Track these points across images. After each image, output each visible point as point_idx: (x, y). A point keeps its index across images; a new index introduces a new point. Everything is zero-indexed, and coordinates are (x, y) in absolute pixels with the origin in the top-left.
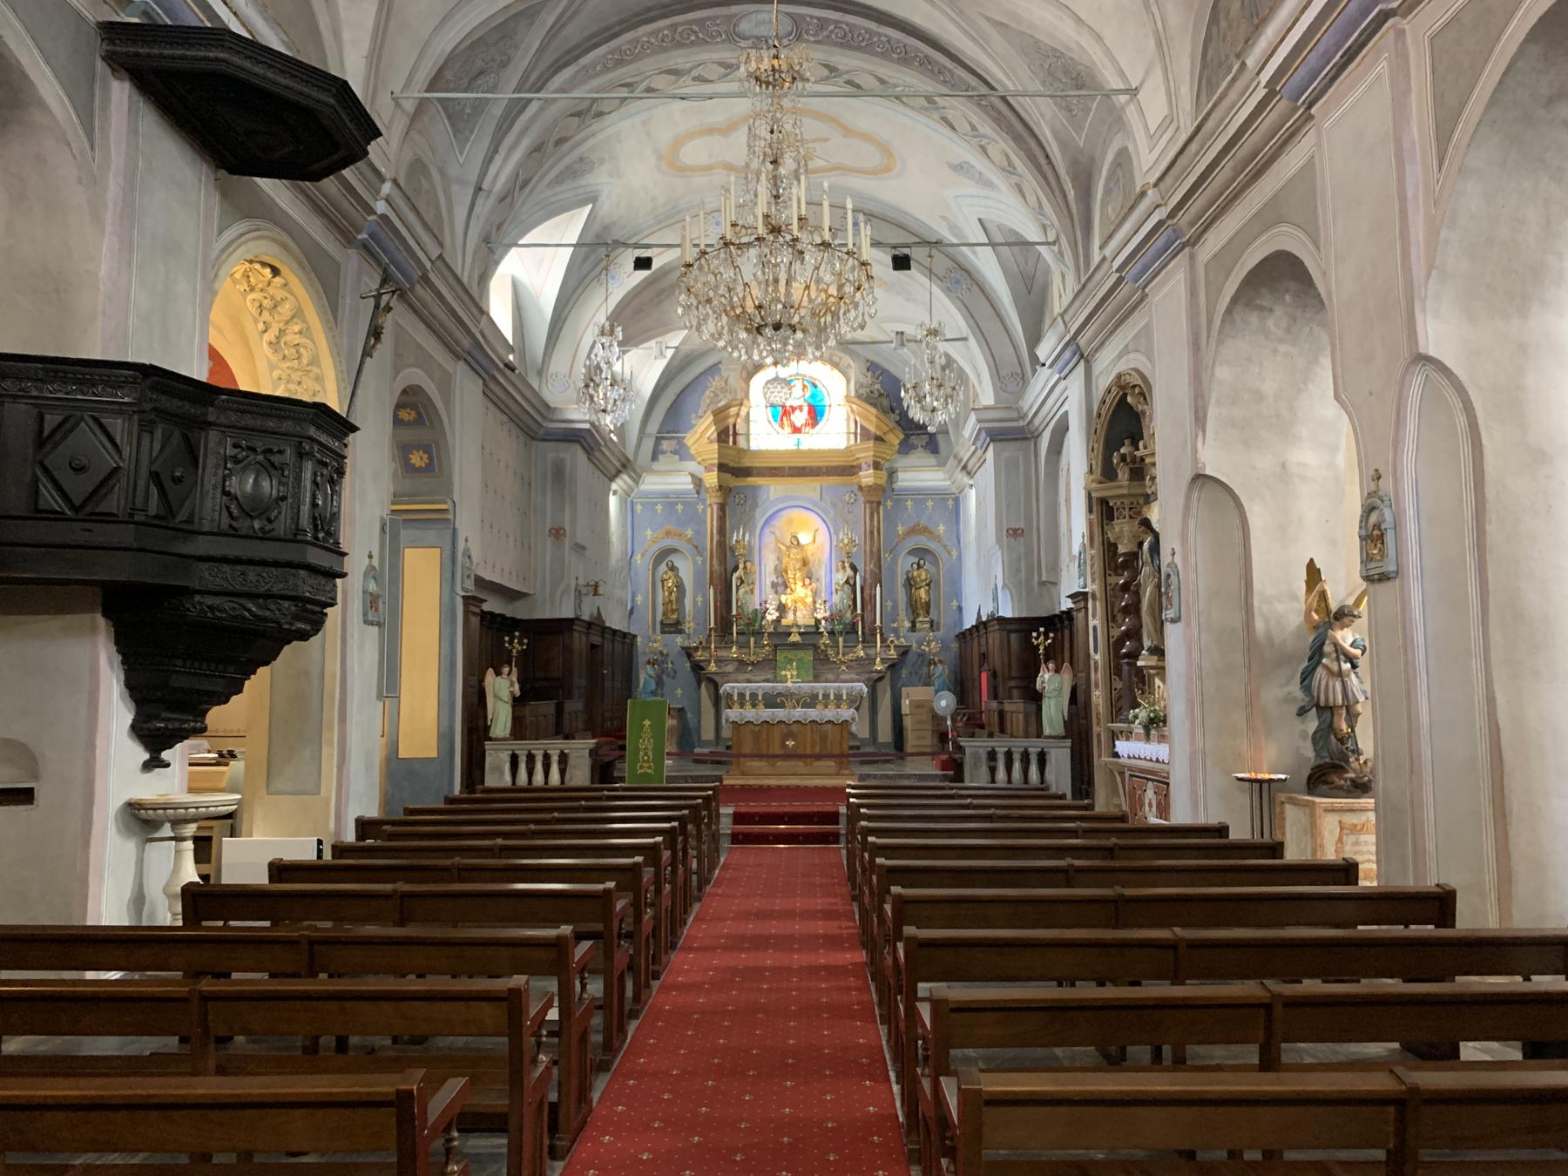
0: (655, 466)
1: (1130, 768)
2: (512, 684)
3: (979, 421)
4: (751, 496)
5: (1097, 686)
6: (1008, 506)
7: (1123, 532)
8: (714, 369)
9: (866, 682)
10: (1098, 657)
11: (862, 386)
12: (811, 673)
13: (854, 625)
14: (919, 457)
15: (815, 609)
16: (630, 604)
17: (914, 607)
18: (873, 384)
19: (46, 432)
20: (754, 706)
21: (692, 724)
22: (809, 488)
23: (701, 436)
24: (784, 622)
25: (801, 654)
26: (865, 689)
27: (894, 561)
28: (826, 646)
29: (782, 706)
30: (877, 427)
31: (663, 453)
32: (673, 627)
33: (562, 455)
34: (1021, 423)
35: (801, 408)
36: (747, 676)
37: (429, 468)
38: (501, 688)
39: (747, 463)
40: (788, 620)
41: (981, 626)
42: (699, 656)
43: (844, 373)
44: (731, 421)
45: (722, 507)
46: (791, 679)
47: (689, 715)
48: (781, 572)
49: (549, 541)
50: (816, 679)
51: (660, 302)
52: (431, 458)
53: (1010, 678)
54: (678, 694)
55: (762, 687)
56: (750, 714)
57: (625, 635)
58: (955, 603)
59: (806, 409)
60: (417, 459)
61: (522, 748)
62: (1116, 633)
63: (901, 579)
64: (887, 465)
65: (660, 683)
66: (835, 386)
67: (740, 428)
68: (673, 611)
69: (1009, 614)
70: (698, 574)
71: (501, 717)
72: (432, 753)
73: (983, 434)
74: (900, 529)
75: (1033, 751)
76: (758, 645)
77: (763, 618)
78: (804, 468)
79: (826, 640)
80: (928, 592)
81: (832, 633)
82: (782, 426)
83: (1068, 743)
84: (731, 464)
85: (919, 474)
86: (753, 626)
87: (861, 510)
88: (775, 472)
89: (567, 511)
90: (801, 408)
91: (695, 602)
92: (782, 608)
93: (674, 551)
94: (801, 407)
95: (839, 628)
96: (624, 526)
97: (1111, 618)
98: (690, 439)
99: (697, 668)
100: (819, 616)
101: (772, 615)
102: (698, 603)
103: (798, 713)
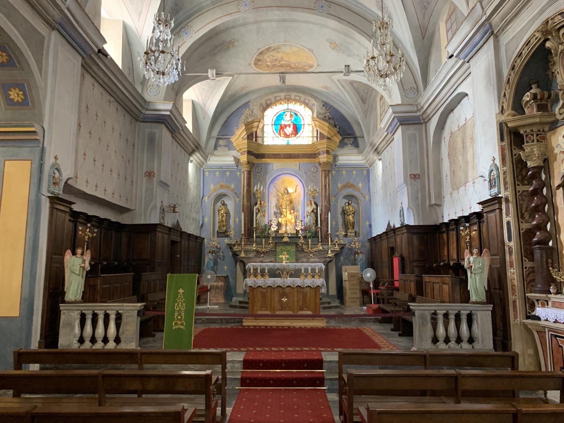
0: (216, 152)
1: (551, 329)
2: (84, 261)
3: (394, 113)
5: (512, 266)
6: (411, 161)
7: (532, 155)
8: (246, 105)
9: (324, 262)
10: (512, 244)
11: (320, 114)
12: (294, 259)
13: (316, 232)
15: (296, 225)
16: (198, 219)
17: (346, 225)
20: (263, 276)
22: (293, 164)
23: (239, 137)
24: (280, 232)
25: (289, 248)
26: (324, 267)
27: (336, 201)
28: (302, 244)
29: (279, 276)
30: (328, 133)
31: (220, 146)
33: (154, 130)
34: (418, 114)
35: (289, 126)
36: (261, 259)
37: (24, 103)
38: (76, 266)
41: (391, 231)
42: (236, 248)
43: (311, 109)
44: (254, 130)
45: (249, 173)
46: (285, 260)
47: (231, 280)
48: (279, 207)
49: (145, 179)
50: (297, 261)
51: (215, 55)
52: (25, 94)
53: (414, 261)
54: (225, 269)
55: (268, 265)
56: (260, 281)
57: (197, 237)
58: (368, 223)
59: (292, 126)
60: (14, 95)
61: (89, 308)
62: (525, 226)
63: (340, 210)
64: (333, 153)
65: (216, 263)
66: (306, 115)
67: (259, 134)
68: (224, 226)
69: (412, 223)
70: (236, 206)
71: (74, 286)
72: (15, 312)
73: (396, 120)
75: (464, 313)
76: (267, 243)
77: (270, 229)
78: (291, 154)
80: (353, 217)
81: (305, 237)
82: (280, 134)
83: (490, 307)
84: (254, 152)
85: (349, 157)
86: (264, 233)
87: (320, 174)
88: (276, 156)
89: (156, 163)
90: (289, 126)
91: (235, 221)
92: (279, 225)
93: (225, 195)
94: (289, 125)
95: (309, 235)
96: (199, 181)
97: (520, 216)
98: (233, 139)
99: (235, 255)
100: (298, 229)
101: (274, 228)
102: (237, 221)
103: (289, 281)
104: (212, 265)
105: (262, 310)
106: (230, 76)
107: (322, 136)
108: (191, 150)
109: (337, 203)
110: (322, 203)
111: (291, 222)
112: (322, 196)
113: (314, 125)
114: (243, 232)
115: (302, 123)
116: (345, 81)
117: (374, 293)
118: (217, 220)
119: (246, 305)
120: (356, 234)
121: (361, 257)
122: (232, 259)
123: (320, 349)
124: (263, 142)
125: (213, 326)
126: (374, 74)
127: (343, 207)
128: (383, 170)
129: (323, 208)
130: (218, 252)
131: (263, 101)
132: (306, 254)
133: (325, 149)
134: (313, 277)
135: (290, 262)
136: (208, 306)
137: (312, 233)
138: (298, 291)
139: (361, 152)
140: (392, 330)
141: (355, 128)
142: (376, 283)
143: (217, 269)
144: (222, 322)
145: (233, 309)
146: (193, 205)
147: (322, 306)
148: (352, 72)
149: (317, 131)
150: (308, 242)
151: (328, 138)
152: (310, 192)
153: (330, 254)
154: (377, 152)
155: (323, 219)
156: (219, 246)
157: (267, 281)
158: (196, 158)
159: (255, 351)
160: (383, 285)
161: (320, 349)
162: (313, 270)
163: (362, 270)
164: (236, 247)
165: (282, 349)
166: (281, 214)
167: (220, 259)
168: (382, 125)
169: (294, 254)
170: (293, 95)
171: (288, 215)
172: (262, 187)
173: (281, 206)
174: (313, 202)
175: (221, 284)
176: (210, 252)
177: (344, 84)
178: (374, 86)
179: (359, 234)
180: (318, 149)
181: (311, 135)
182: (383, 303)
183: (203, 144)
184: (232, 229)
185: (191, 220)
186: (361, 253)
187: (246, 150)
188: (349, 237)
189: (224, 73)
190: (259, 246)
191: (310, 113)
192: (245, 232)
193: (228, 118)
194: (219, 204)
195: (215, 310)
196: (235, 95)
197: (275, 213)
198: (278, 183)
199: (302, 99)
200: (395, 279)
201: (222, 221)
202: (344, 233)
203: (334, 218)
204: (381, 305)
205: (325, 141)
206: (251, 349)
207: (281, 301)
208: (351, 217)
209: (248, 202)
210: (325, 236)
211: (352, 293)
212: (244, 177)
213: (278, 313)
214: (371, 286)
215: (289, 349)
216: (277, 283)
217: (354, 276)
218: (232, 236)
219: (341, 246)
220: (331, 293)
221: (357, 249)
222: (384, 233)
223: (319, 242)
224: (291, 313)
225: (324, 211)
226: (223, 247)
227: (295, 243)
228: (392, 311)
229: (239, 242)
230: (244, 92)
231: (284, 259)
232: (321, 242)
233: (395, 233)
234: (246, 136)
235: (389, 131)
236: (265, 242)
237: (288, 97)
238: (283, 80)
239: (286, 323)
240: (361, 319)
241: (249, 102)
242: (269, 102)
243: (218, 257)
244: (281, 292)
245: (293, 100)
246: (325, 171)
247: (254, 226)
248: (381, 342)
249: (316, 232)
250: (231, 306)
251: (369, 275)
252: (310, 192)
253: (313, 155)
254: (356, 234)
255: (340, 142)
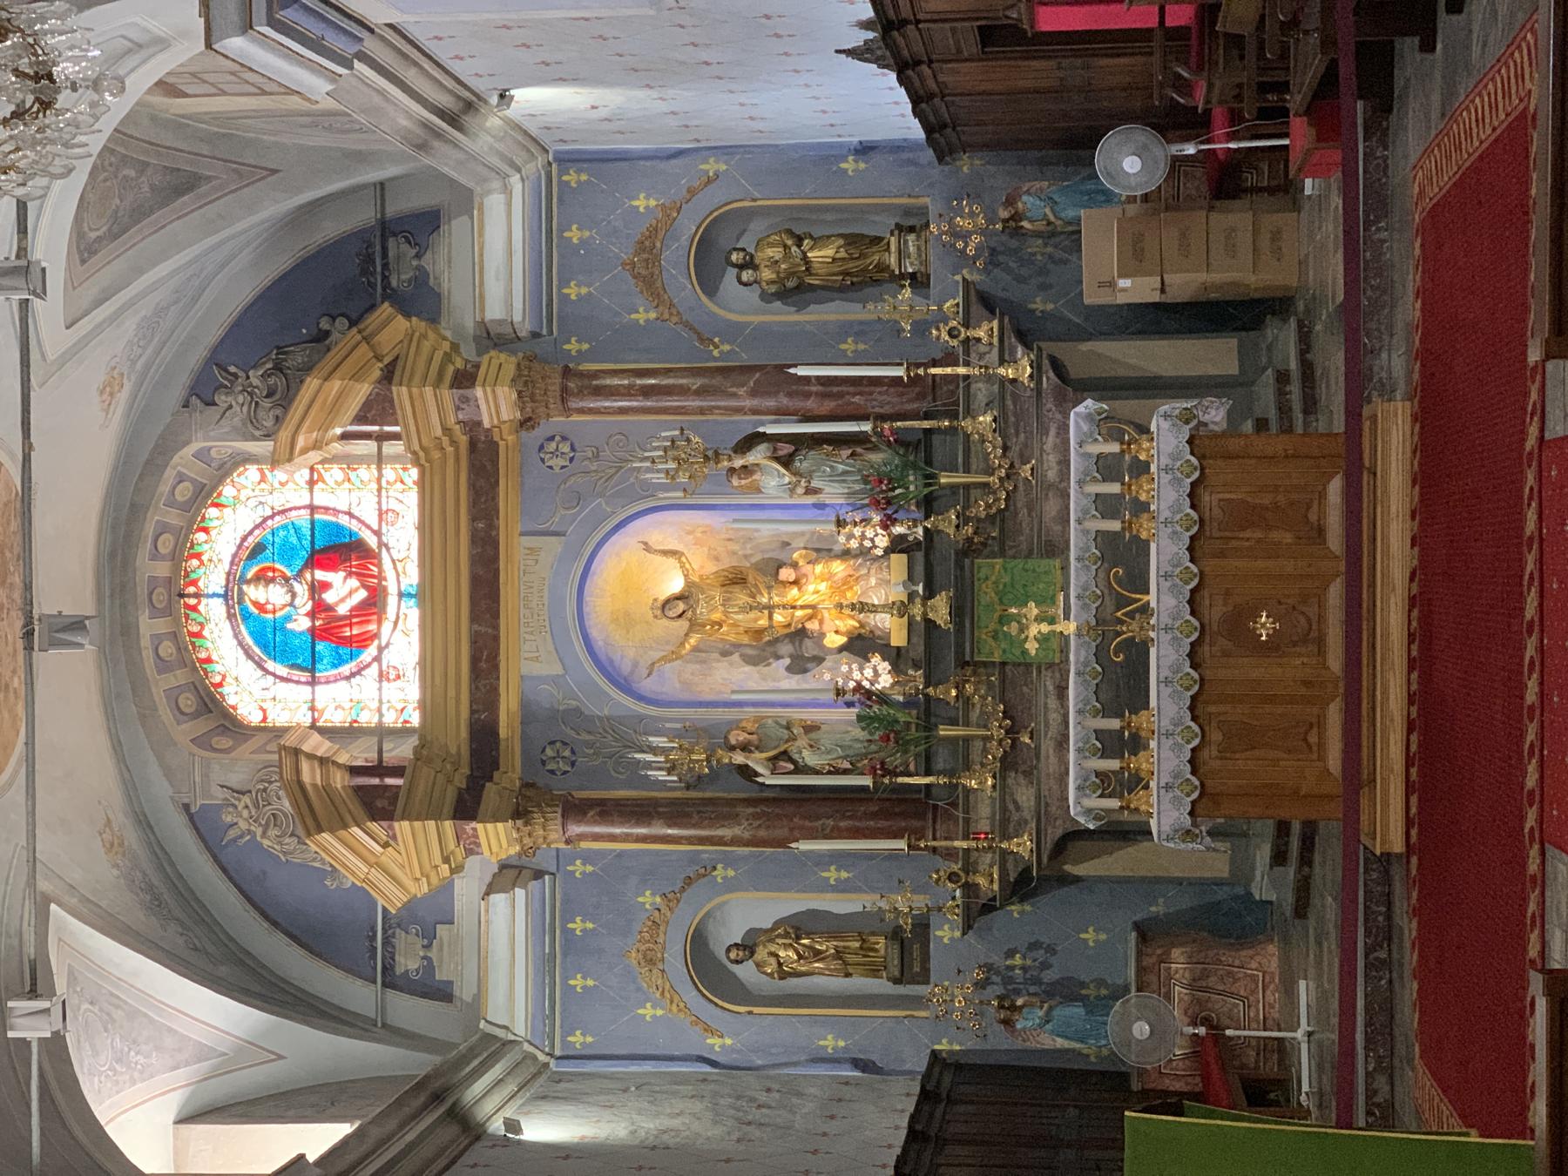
0: (464, 992)
3: (247, 26)
4: (556, 728)
8: (201, 823)
11: (253, 420)
12: (1045, 564)
13: (902, 442)
14: (446, 264)
15: (864, 553)
17: (859, 279)
18: (248, 390)
19: (205, 77)
20: (1136, 744)
21: (1186, 902)
22: (529, 564)
23: (385, 866)
24: (898, 639)
25: (986, 594)
26: (1089, 405)
27: (732, 332)
28: (963, 519)
29: (1138, 653)
30: (356, 376)
32: (909, 951)
35: (318, 588)
36: (1048, 747)
39: (458, 738)
40: (895, 630)
42: (988, 882)
43: (225, 469)
44: (339, 780)
45: (575, 809)
46: (1052, 622)
48: (762, 647)
50: (1055, 548)
54: (1096, 940)
55: (1077, 713)
56: (1165, 759)
57: (927, 1096)
58: (849, 165)
59: (320, 575)
63: (783, 315)
65: (1066, 991)
66: (256, 499)
67: (361, 754)
68: (866, 949)
74: (644, 315)
76: (961, 712)
77: (883, 698)
78: (475, 581)
79: (947, 522)
80: (818, 241)
81: (929, 505)
82: (363, 641)
84: (460, 781)
85: (494, 262)
86: (906, 727)
87: (586, 422)
88: (485, 659)
90: (318, 588)
91: (841, 888)
92: (861, 645)
93: (698, 942)
94: (316, 580)
95: (914, 484)
96: (624, 1086)
98: (391, 897)
99: (1022, 886)
100: (883, 542)
101: (879, 674)
102: (841, 877)
103: (1164, 599)
104: (1077, 1011)
105: (1321, 745)
106: (43, 917)
107: (377, 410)
108: (453, 1130)
109: (741, 327)
110: (742, 411)
111: (847, 585)
112: (702, 411)
113: (314, 456)
114: (901, 844)
115: (302, 519)
116: (72, 284)
117: (1231, 137)
118: (836, 984)
119: (1296, 827)
120: (912, 224)
121: (1037, 203)
122: (1043, 900)
123: (1531, 443)
124: (404, 732)
125: (1408, 1016)
126: (34, 143)
127: (766, 297)
128: (561, 80)
129: (771, 403)
130: (1008, 980)
131: (184, 732)
132: (1021, 499)
133: (447, 395)
134: (1141, 468)
135: (1065, 588)
136: (1299, 1035)
137: (906, 466)
138: (1222, 554)
139: (466, 201)
140: (1428, 46)
141: (330, 229)
142: (1174, 122)
143: (1100, 983)
144: (1387, 964)
145: (1315, 901)
146: (755, 1114)
147: (1298, 417)
148: (22, 252)
149: (346, 436)
150: (954, 488)
151: (388, 376)
152: (683, 479)
153: (1021, 369)
154: (461, 111)
155: (829, 406)
156: (978, 975)
157: (1166, 723)
158: (493, 1103)
159: (1541, 797)
160: (1185, 87)
161: (1531, 443)
162: (1107, 468)
163: (1108, 197)
164: (981, 881)
165: (1530, 652)
166: (801, 633)
167: (1045, 966)
168: (317, 87)
169: (1019, 563)
170: (150, 568)
171: (808, 598)
172: (656, 741)
173: (759, 633)
174: (738, 463)
175: (1179, 963)
176: (1007, 1022)
177: (90, 291)
178: (96, 143)
179: (907, 211)
180: (447, 430)
181: (366, 473)
182: (1283, 87)
183: (418, 1063)
184: (884, 905)
185: (832, 1127)
186: (1010, 202)
187: (448, 825)
188: (925, 263)
189: (30, 950)
190: (975, 756)
191: (252, 472)
192: (896, 835)
193: (275, 924)
194: (746, 972)
195: (1322, 997)
196: (150, 888)
197: (799, 666)
198: (631, 653)
199: (174, 518)
200: (1153, 22)
201: (839, 955)
202: (907, 293)
203: (823, 346)
204: (1295, 101)
205: (400, 393)
206: (1531, 820)
207: (1272, 648)
208: (820, 255)
209: (733, 818)
210: (921, 396)
211: (1226, 253)
212: (597, 838)
213: (1335, 662)
214: (1190, 150)
215: (1530, 611)
216: (1176, 669)
217: (1138, 240)
218: (921, 901)
219: (977, 309)
220: (1232, 368)
221: (991, 221)
222: (901, 81)
223: (953, 430)
224: (1335, 593)
225: (785, 401)
226: (978, 948)
227: (961, 555)
228: (1328, 43)
229: (956, 867)
230: (132, 837)
231: (1045, 628)
232: (953, 416)
233: (904, 23)
234: (373, 826)
235: (350, 49)
236: (953, 722)
237: (160, 596)
238: (69, 628)
239: (1393, 619)
240: (1366, 209)
241: (186, 807)
242: (188, 702)
243: (1037, 981)
244: (1223, 643)
245: (176, 568)
246: (565, 393)
247: (867, 781)
248: (1494, 107)
249: (902, 442)
250: (1301, 910)
251: (1129, 161)
252: (683, 479)
253: (481, 458)
254: (912, 224)
255: (407, 315)
